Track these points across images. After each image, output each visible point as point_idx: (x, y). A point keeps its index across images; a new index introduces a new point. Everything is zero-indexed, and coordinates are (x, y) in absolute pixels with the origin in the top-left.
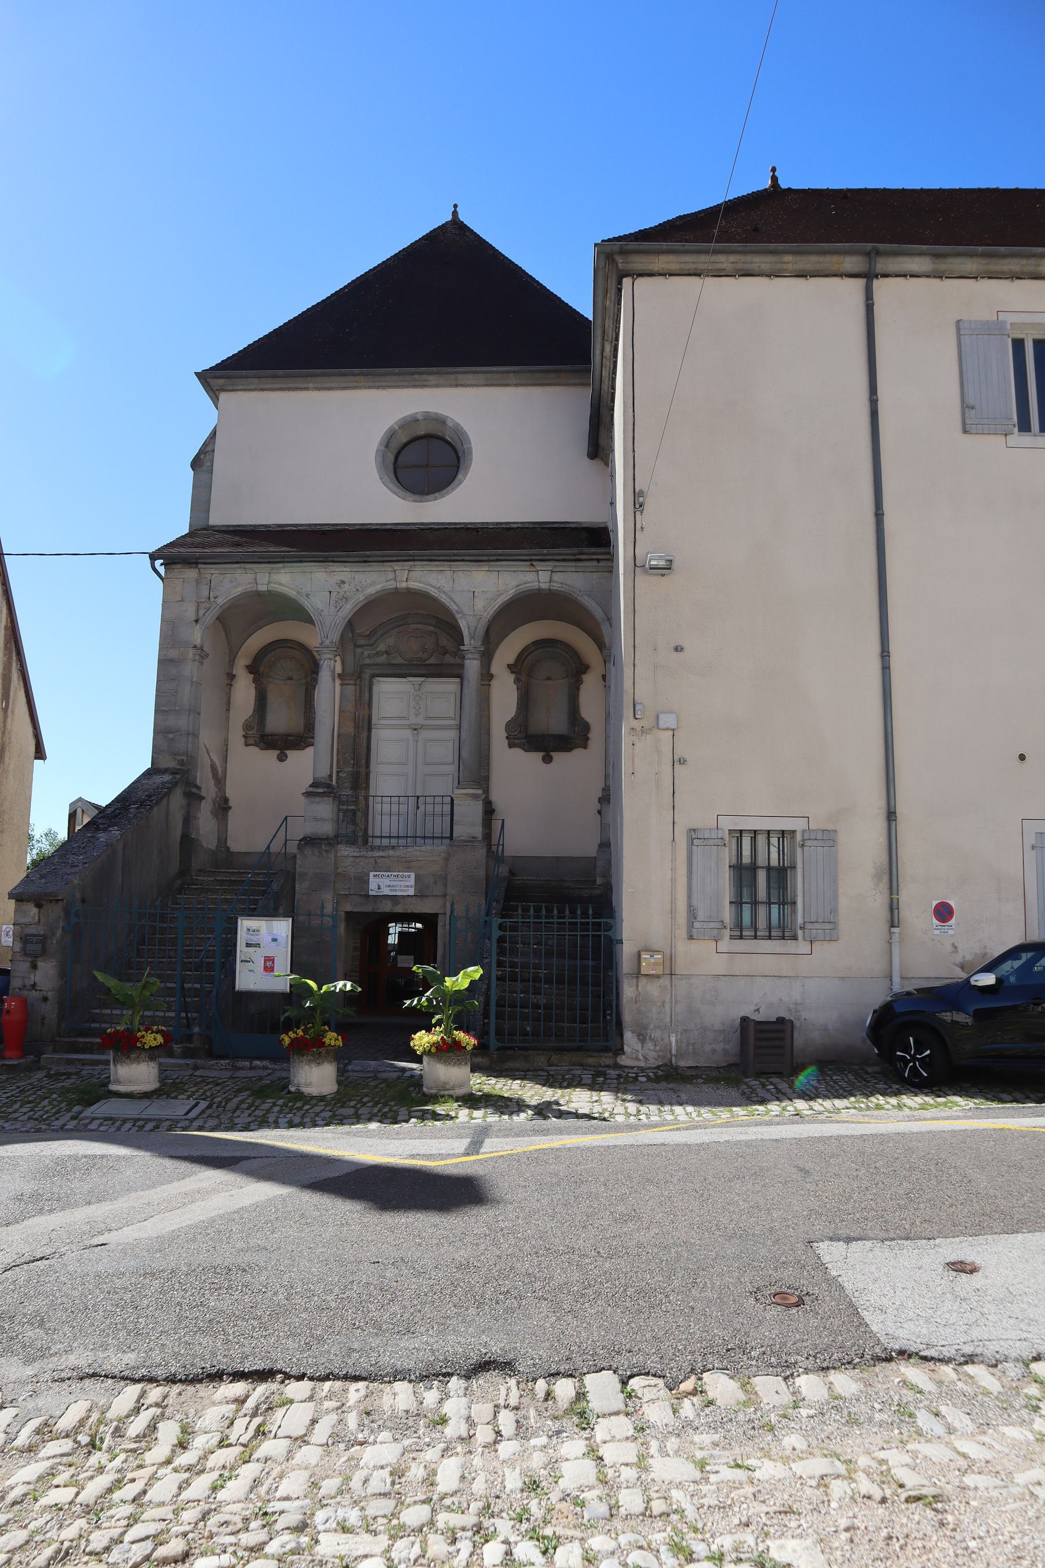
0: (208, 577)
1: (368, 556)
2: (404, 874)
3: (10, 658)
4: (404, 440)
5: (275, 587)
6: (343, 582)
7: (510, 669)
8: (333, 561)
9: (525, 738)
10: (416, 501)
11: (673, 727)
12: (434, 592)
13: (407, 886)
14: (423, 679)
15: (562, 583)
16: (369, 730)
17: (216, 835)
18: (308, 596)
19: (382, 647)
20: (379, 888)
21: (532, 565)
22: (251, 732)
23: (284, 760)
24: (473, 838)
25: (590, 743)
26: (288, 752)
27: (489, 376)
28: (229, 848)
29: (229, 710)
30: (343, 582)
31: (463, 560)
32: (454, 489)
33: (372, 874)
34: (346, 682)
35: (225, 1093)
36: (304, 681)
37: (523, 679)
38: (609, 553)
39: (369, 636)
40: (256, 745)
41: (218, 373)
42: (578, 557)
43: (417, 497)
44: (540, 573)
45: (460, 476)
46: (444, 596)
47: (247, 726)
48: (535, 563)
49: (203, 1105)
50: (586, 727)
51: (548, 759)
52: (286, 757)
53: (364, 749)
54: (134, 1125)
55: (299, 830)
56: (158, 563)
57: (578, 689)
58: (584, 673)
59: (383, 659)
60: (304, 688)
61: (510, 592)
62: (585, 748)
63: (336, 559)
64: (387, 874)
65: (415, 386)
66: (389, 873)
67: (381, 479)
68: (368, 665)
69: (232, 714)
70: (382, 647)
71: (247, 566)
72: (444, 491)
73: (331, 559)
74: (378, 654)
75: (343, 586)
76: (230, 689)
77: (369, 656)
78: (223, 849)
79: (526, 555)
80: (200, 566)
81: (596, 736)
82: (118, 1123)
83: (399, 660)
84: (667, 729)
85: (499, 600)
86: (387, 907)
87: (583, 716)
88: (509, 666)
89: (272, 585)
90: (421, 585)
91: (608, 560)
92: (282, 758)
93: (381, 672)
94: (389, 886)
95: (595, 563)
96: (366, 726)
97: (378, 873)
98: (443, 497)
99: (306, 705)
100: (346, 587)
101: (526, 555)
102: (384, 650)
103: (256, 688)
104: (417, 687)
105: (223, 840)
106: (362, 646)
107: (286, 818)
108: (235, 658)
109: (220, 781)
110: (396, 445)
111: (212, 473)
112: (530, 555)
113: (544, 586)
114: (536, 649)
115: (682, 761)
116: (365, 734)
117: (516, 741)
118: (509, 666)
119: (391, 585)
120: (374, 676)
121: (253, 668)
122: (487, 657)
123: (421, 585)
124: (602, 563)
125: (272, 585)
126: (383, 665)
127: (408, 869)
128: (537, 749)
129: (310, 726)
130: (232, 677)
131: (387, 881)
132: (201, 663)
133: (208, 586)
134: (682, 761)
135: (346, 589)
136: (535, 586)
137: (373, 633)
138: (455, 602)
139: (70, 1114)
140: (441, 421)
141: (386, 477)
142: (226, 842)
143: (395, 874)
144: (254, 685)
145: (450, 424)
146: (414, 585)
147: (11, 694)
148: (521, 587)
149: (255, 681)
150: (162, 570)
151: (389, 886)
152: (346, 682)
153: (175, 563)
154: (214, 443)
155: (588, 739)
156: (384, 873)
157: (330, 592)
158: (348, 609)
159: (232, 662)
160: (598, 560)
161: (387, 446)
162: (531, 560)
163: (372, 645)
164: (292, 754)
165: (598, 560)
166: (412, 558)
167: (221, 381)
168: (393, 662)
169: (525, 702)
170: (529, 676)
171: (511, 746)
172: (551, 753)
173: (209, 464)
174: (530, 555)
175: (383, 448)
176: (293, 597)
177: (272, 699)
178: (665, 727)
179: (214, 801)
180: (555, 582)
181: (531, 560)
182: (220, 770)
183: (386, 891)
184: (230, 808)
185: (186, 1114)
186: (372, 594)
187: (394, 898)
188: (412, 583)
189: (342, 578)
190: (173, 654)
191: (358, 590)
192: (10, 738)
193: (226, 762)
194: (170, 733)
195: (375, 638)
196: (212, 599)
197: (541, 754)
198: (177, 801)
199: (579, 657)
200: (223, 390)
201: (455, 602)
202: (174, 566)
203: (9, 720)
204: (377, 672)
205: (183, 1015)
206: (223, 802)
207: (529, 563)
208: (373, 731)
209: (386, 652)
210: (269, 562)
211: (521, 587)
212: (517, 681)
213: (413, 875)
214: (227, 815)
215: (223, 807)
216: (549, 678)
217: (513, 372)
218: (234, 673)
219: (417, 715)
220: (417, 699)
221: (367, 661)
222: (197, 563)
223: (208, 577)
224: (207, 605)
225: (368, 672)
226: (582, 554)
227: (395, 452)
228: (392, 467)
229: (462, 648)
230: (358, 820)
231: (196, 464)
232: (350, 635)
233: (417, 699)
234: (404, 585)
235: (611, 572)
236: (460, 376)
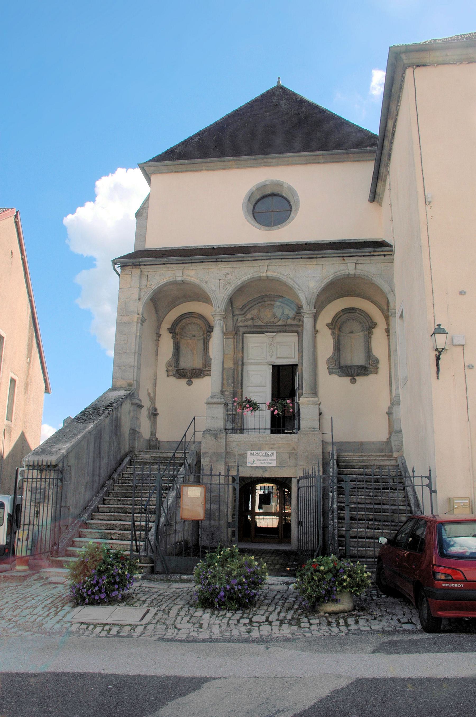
0: (146, 273)
1: (243, 257)
2: (270, 452)
3: (32, 335)
4: (258, 197)
5: (186, 278)
6: (228, 274)
7: (328, 326)
8: (222, 261)
9: (339, 368)
10: (267, 230)
11: (462, 343)
12: (284, 278)
13: (272, 460)
14: (275, 334)
15: (362, 270)
16: (243, 365)
17: (150, 431)
18: (206, 282)
19: (249, 316)
20: (254, 462)
21: (344, 260)
22: (170, 368)
23: (191, 385)
24: (313, 428)
25: (380, 371)
26: (193, 380)
27: (308, 158)
28: (157, 439)
29: (157, 355)
30: (228, 274)
31: (301, 258)
32: (289, 222)
33: (249, 453)
34: (228, 337)
35: (166, 601)
36: (202, 337)
37: (336, 332)
38: (392, 251)
39: (242, 309)
40: (174, 376)
41: (151, 164)
42: (372, 254)
43: (267, 228)
44: (348, 264)
45: (292, 215)
46: (290, 280)
47: (168, 365)
48: (345, 258)
49: (153, 611)
50: (377, 361)
51: (353, 381)
52: (192, 382)
53: (240, 379)
54: (103, 630)
55: (202, 425)
56: (116, 266)
57: (370, 338)
58: (374, 328)
59: (250, 322)
60: (202, 341)
61: (331, 277)
62: (376, 374)
63: (223, 260)
64: (258, 452)
65: (265, 166)
66: (260, 452)
67: (246, 218)
68: (241, 326)
69: (159, 357)
70: (249, 316)
71: (170, 265)
72: (284, 224)
73: (220, 260)
74: (247, 320)
75: (228, 276)
76: (158, 343)
77: (241, 321)
78: (154, 439)
79: (339, 253)
80: (141, 267)
81: (383, 366)
82: (91, 627)
83: (260, 323)
84: (459, 345)
85: (324, 281)
86: (259, 474)
87: (374, 354)
88: (328, 325)
89: (185, 277)
90: (275, 274)
91: (391, 255)
92: (190, 383)
93: (249, 330)
94: (260, 460)
95: (383, 257)
96: (240, 363)
97: (252, 452)
98: (283, 227)
99: (204, 351)
100: (229, 277)
101: (339, 253)
102: (251, 317)
103: (174, 342)
104: (271, 339)
105: (153, 434)
106: (237, 315)
107: (194, 418)
108: (161, 324)
109: (152, 399)
110: (254, 200)
111: (147, 219)
112: (342, 253)
113: (352, 272)
114: (344, 314)
115: (471, 367)
116: (240, 368)
117: (333, 370)
118: (328, 325)
119: (257, 275)
120: (244, 333)
121: (172, 330)
122: (316, 317)
123: (275, 274)
124: (387, 257)
125: (185, 277)
126: (251, 326)
127: (271, 449)
128: (348, 375)
129: (207, 363)
130: (159, 335)
131: (259, 457)
132: (142, 325)
133: (146, 279)
134: (471, 367)
135: (229, 278)
136: (346, 272)
137: (244, 307)
138: (297, 284)
139: (57, 618)
140: (280, 185)
141: (249, 217)
142: (155, 435)
143: (264, 452)
144: (172, 340)
145: (286, 186)
146: (270, 274)
147: (32, 354)
148: (337, 273)
149: (173, 337)
150: (119, 270)
151: (260, 460)
152: (228, 337)
153: (127, 266)
154: (148, 203)
155: (378, 368)
156: (257, 452)
157: (220, 280)
158: (230, 290)
159: (159, 327)
160: (385, 255)
161: (249, 200)
162: (343, 257)
163: (243, 314)
164: (196, 382)
165: (385, 255)
166: (269, 258)
167: (152, 169)
168: (256, 324)
169: (338, 347)
170: (340, 331)
171: (330, 373)
172: (355, 377)
173: (145, 215)
174: (342, 253)
175: (254, 190)
176: (197, 283)
177: (183, 349)
178: (457, 343)
179: (149, 410)
180: (358, 270)
181: (343, 257)
182: (152, 395)
183: (258, 464)
184: (158, 414)
185: (142, 619)
186: (246, 281)
187: (264, 468)
188: (270, 273)
189: (227, 271)
190: (126, 319)
191: (236, 278)
192: (31, 380)
193: (156, 386)
194: (123, 366)
195: (245, 310)
196: (148, 286)
197: (350, 378)
198: (127, 407)
199: (371, 319)
200: (155, 173)
201: (297, 284)
202: (126, 268)
203: (31, 369)
204: (246, 330)
205: (134, 543)
206: (154, 410)
207: (341, 258)
208: (244, 367)
209: (252, 319)
210: (183, 263)
211: (337, 273)
212: (333, 333)
213: (275, 453)
214: (156, 419)
215: (154, 414)
216: (351, 332)
217: (323, 155)
218: (160, 333)
219: (271, 357)
220: (271, 346)
221: (241, 324)
222: (140, 265)
223: (146, 273)
224: (145, 290)
225: (241, 330)
226: (375, 251)
227: (254, 203)
228: (252, 212)
229: (302, 311)
230: (236, 421)
231: (138, 215)
232: (231, 308)
233: (271, 346)
234: (265, 274)
235: (393, 262)
236: (290, 159)
